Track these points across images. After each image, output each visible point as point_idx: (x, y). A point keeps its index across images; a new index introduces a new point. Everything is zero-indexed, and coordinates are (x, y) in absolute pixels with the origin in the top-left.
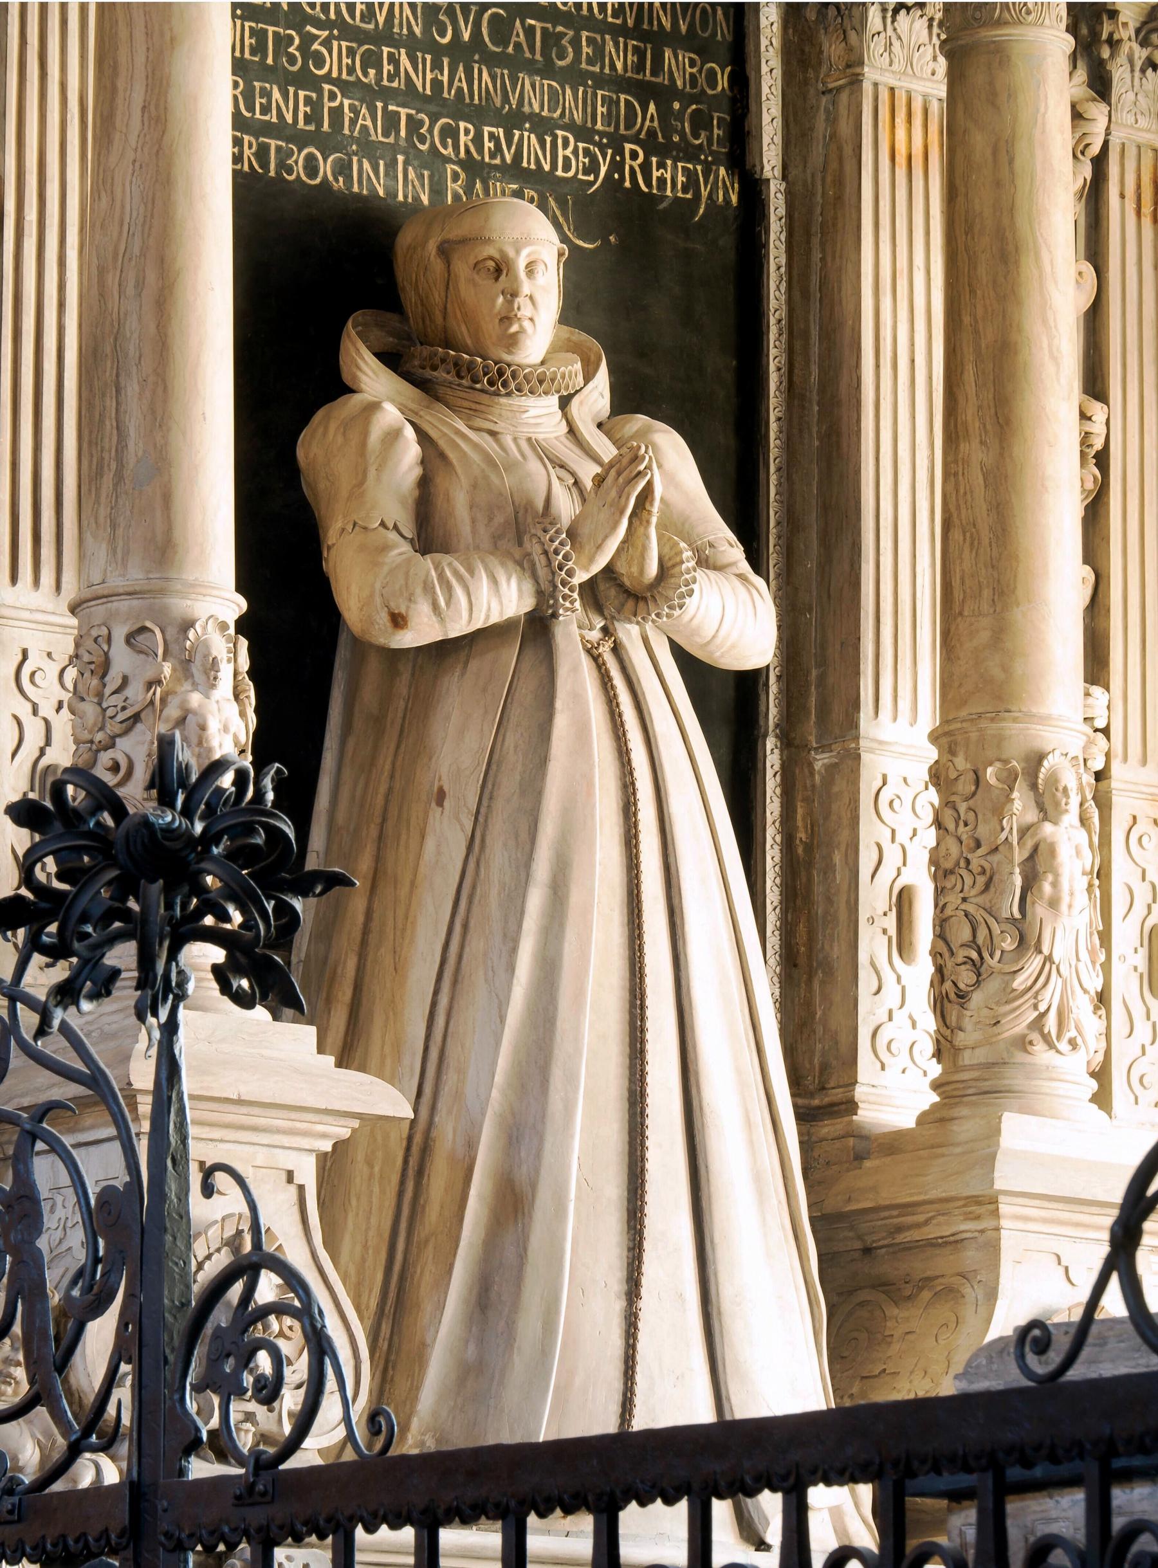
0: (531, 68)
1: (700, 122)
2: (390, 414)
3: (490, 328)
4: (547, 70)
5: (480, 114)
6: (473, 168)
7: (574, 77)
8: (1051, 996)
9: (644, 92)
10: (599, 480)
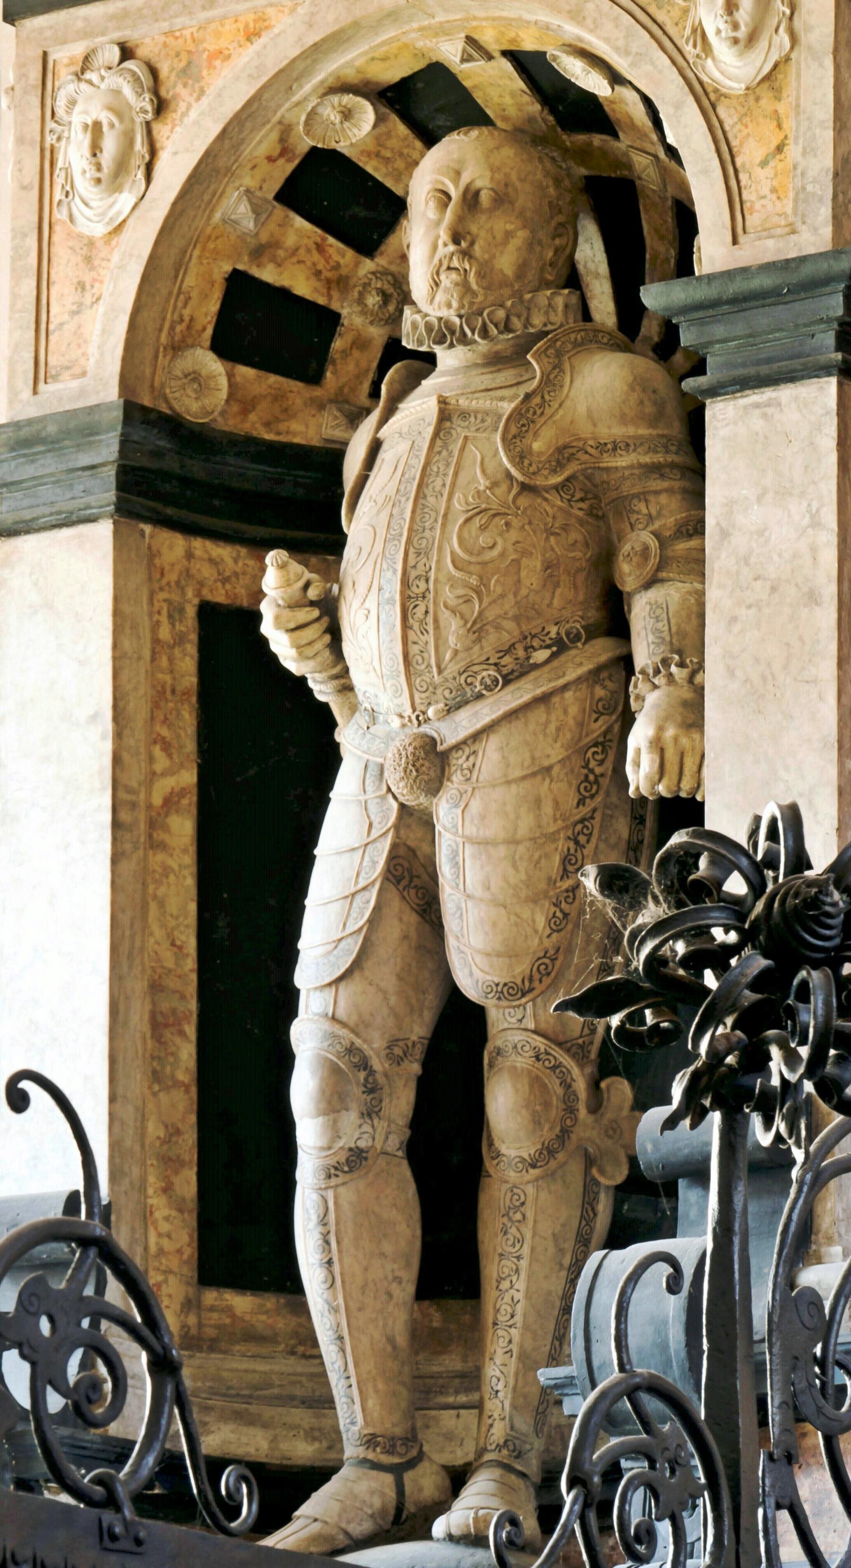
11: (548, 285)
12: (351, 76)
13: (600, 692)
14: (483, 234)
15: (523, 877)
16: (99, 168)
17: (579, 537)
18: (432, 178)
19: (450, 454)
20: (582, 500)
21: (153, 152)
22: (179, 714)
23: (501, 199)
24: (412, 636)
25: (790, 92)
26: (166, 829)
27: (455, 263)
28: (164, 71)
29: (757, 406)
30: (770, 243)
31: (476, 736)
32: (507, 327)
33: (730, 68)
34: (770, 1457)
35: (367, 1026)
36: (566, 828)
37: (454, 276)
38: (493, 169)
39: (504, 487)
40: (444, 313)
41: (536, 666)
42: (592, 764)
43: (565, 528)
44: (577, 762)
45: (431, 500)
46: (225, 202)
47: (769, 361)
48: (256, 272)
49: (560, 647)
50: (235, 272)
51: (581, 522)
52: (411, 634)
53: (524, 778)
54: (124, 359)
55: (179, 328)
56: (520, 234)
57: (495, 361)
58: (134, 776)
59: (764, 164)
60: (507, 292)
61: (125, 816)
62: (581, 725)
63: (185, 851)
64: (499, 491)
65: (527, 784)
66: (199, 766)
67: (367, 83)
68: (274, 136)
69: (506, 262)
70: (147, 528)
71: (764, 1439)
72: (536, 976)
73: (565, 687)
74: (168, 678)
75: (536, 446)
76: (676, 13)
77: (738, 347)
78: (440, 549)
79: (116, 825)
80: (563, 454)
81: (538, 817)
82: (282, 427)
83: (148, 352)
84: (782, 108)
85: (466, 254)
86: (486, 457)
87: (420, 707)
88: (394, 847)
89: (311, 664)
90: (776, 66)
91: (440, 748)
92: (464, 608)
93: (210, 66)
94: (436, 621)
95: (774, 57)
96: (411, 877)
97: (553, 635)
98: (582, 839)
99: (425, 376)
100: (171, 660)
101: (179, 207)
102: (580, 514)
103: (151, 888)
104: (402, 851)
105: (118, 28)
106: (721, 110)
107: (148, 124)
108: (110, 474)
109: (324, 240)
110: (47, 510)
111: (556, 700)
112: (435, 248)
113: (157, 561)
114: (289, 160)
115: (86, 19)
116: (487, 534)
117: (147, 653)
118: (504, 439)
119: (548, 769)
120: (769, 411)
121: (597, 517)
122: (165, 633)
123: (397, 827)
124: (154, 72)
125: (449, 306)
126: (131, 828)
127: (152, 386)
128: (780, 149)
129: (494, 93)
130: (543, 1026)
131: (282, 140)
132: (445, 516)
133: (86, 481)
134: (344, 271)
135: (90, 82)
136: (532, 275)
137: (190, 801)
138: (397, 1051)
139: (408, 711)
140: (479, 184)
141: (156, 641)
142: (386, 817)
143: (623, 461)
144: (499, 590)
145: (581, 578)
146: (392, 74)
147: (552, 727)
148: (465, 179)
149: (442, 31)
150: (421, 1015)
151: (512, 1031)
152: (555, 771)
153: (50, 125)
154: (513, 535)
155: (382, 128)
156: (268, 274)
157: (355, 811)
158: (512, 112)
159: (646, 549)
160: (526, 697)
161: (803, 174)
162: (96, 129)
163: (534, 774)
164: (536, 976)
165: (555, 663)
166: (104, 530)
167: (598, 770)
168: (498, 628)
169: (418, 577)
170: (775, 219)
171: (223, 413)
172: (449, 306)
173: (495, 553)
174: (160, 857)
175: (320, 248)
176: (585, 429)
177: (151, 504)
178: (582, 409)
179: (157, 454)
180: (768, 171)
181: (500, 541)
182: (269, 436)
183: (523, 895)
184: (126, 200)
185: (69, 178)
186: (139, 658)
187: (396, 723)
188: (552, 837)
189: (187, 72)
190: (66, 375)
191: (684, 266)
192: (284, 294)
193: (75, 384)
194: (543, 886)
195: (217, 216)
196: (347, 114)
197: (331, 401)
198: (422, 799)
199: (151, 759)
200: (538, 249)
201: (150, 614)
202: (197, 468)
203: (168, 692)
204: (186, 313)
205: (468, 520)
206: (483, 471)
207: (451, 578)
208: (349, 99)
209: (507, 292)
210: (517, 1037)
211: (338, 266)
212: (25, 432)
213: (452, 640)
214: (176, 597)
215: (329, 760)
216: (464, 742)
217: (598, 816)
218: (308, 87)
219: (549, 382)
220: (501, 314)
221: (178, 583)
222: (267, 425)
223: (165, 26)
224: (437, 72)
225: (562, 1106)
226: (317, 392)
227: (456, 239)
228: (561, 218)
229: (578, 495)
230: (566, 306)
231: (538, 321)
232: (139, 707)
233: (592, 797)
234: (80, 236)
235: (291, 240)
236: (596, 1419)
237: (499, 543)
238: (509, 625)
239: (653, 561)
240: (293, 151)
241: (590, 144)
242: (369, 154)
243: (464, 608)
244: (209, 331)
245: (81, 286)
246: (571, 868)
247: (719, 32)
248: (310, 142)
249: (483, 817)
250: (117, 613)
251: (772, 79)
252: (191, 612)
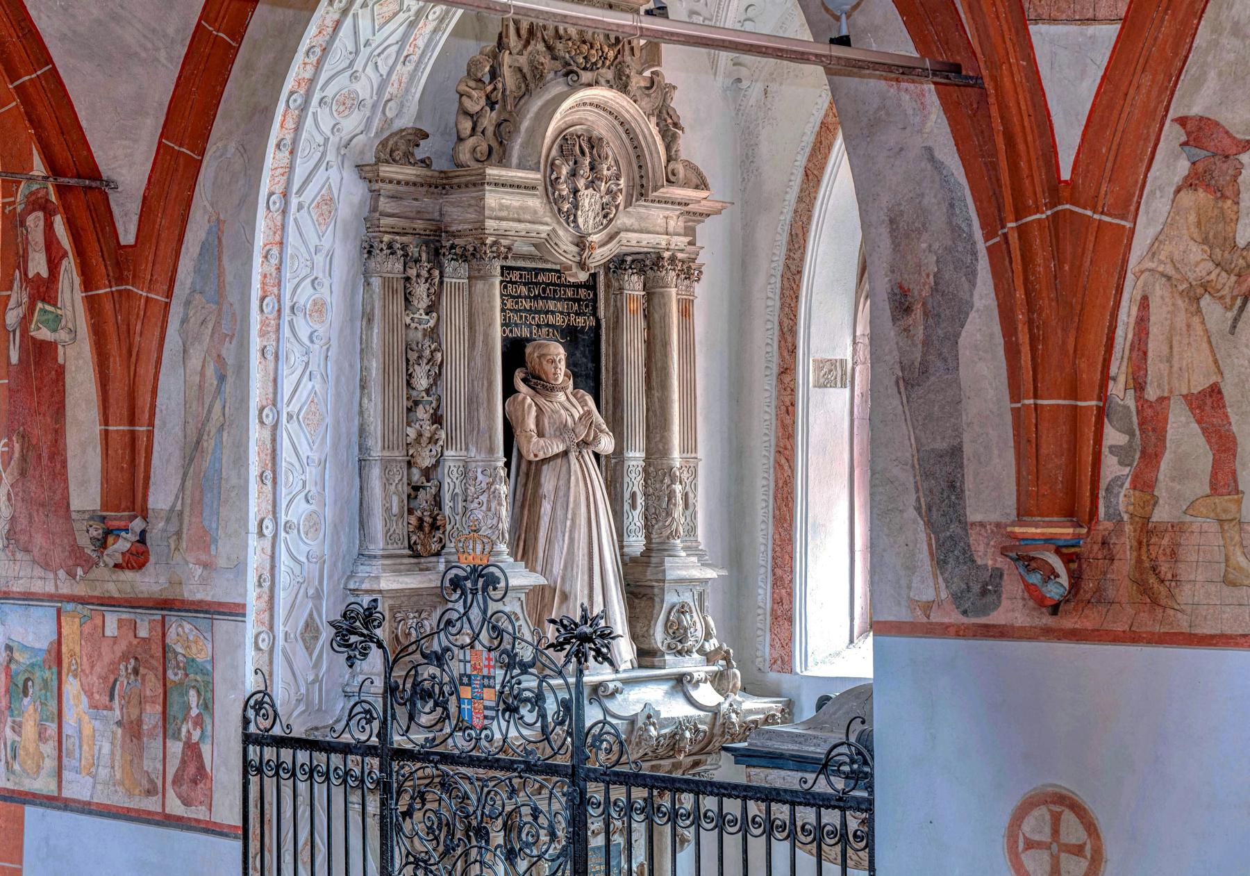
0: (550, 298)
1: (587, 306)
2: (529, 400)
3: (551, 376)
4: (554, 299)
5: (539, 312)
6: (539, 326)
7: (560, 299)
8: (674, 526)
9: (574, 300)
10: (580, 419)
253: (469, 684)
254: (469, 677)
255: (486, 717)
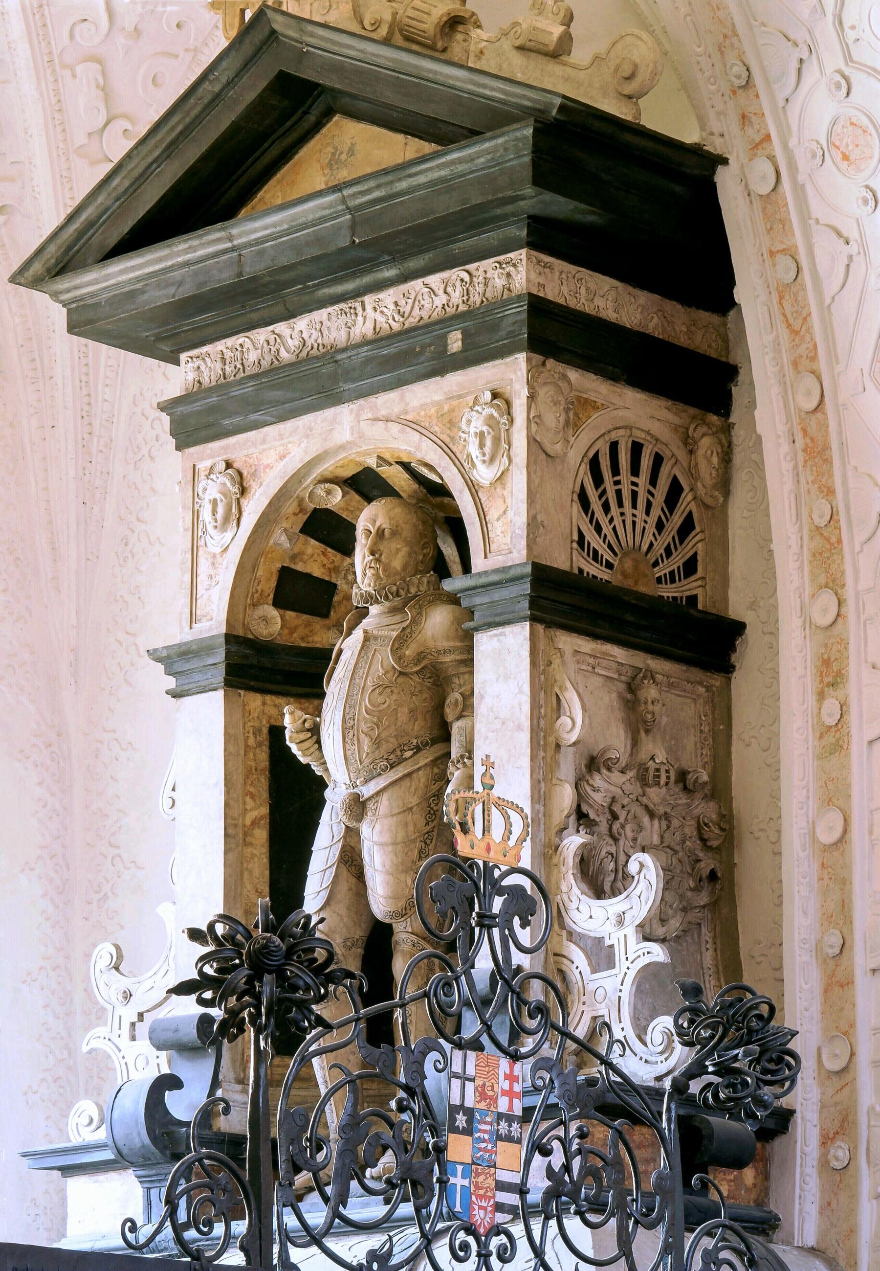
11: (421, 572)
12: (329, 475)
13: (436, 770)
14: (386, 550)
15: (400, 860)
16: (216, 521)
17: (428, 696)
18: (369, 518)
19: (368, 657)
20: (430, 678)
21: (240, 513)
22: (259, 780)
23: (394, 533)
24: (347, 746)
25: (508, 485)
26: (252, 836)
27: (372, 565)
28: (245, 474)
29: (495, 635)
30: (500, 558)
31: (378, 794)
32: (398, 595)
33: (484, 474)
34: (280, 1184)
35: (333, 932)
36: (420, 836)
37: (372, 571)
38: (390, 519)
39: (391, 673)
40: (368, 589)
41: (406, 759)
42: (432, 805)
43: (420, 692)
44: (425, 804)
45: (358, 680)
46: (274, 536)
47: (501, 614)
48: (293, 566)
49: (418, 749)
50: (283, 566)
51: (429, 689)
52: (347, 745)
53: (399, 813)
54: (228, 612)
55: (256, 596)
56: (404, 549)
57: (393, 611)
58: (236, 812)
59: (498, 519)
60: (398, 577)
61: (230, 831)
62: (427, 787)
63: (263, 846)
64: (388, 676)
65: (401, 816)
66: (270, 804)
67: (337, 477)
68: (295, 504)
69: (397, 564)
70: (242, 692)
71: (276, 1177)
72: (408, 908)
73: (419, 769)
74: (253, 764)
75: (407, 653)
76: (461, 447)
77: (487, 607)
78: (360, 705)
79: (226, 835)
80: (420, 656)
81: (406, 832)
82: (310, 639)
83: (241, 608)
84: (505, 493)
85: (378, 560)
86: (384, 659)
87: (353, 780)
88: (343, 846)
89: (310, 758)
90: (503, 473)
91: (361, 800)
92: (370, 733)
93: (265, 472)
94: (358, 739)
95: (502, 469)
96: (351, 860)
97: (414, 744)
98: (428, 841)
99: (364, 618)
100: (254, 755)
101: (252, 539)
102: (428, 684)
103: (245, 865)
104: (348, 848)
105: (225, 454)
106: (480, 494)
107: (238, 499)
108: (222, 668)
109: (326, 550)
110: (194, 685)
111: (415, 775)
112: (364, 557)
113: (247, 708)
114: (305, 514)
115: (211, 449)
116: (382, 697)
117: (242, 752)
118: (391, 650)
119: (411, 809)
120: (501, 638)
121: (437, 685)
122: (251, 742)
123: (345, 837)
124: (240, 474)
125: (370, 586)
126: (235, 836)
127: (244, 624)
128: (505, 512)
129: (396, 480)
130: (415, 930)
131: (299, 505)
132: (363, 688)
133: (213, 671)
134: (336, 564)
135: (212, 480)
136: (411, 569)
137: (265, 822)
138: (349, 944)
139: (348, 782)
140: (384, 526)
141: (247, 746)
142: (340, 832)
143: (448, 659)
144: (387, 723)
145: (428, 717)
146: (348, 473)
147: (413, 789)
148: (378, 524)
149: (367, 453)
150: (360, 926)
151: (404, 934)
152: (415, 808)
153: (197, 500)
154: (394, 697)
155: (348, 497)
156: (300, 567)
157: (328, 828)
158: (406, 488)
159: (457, 701)
160: (400, 775)
161: (514, 525)
162: (214, 502)
163: (404, 811)
164: (408, 908)
165: (415, 757)
166: (220, 694)
167: (435, 808)
168: (387, 742)
169: (350, 718)
170: (503, 547)
171: (279, 634)
172: (370, 586)
173: (385, 706)
174: (250, 849)
175: (324, 554)
176: (431, 644)
177: (243, 680)
178: (429, 633)
179: (246, 656)
180: (500, 523)
181: (387, 700)
182: (303, 645)
183: (400, 868)
184: (229, 535)
185: (205, 526)
186: (238, 755)
187: (344, 787)
188: (414, 841)
189: (254, 475)
190: (204, 619)
191: (466, 567)
192: (308, 576)
193: (208, 623)
194: (409, 864)
195: (272, 542)
196: (329, 492)
197: (334, 626)
198: (355, 824)
199: (245, 803)
200: (414, 556)
201: (244, 734)
202: (266, 662)
203: (254, 771)
204: (259, 588)
205: (373, 691)
206: (382, 666)
207: (365, 718)
208: (328, 485)
209: (398, 577)
210: (404, 936)
211: (333, 561)
212: (184, 648)
213: (366, 748)
214: (257, 724)
215: (321, 803)
216: (372, 796)
217: (436, 830)
218: (309, 481)
219: (415, 621)
220: (394, 588)
221: (258, 717)
222: (302, 639)
223: (245, 452)
224: (368, 470)
225: (427, 968)
226: (327, 622)
227: (372, 553)
228: (426, 540)
229: (428, 675)
230: (428, 582)
231: (413, 590)
232: (238, 778)
233: (432, 821)
234: (210, 553)
235: (310, 551)
236: (178, 1174)
237: (387, 701)
238: (392, 740)
239: (460, 707)
240: (306, 510)
241: (443, 502)
242: (343, 509)
243: (370, 733)
244: (272, 596)
245: (211, 577)
246: (423, 856)
247: (477, 457)
248: (313, 506)
249: (381, 832)
250: (226, 734)
251: (501, 479)
252: (265, 731)
253: (468, 1131)
254: (469, 1113)
255: (500, 1207)
